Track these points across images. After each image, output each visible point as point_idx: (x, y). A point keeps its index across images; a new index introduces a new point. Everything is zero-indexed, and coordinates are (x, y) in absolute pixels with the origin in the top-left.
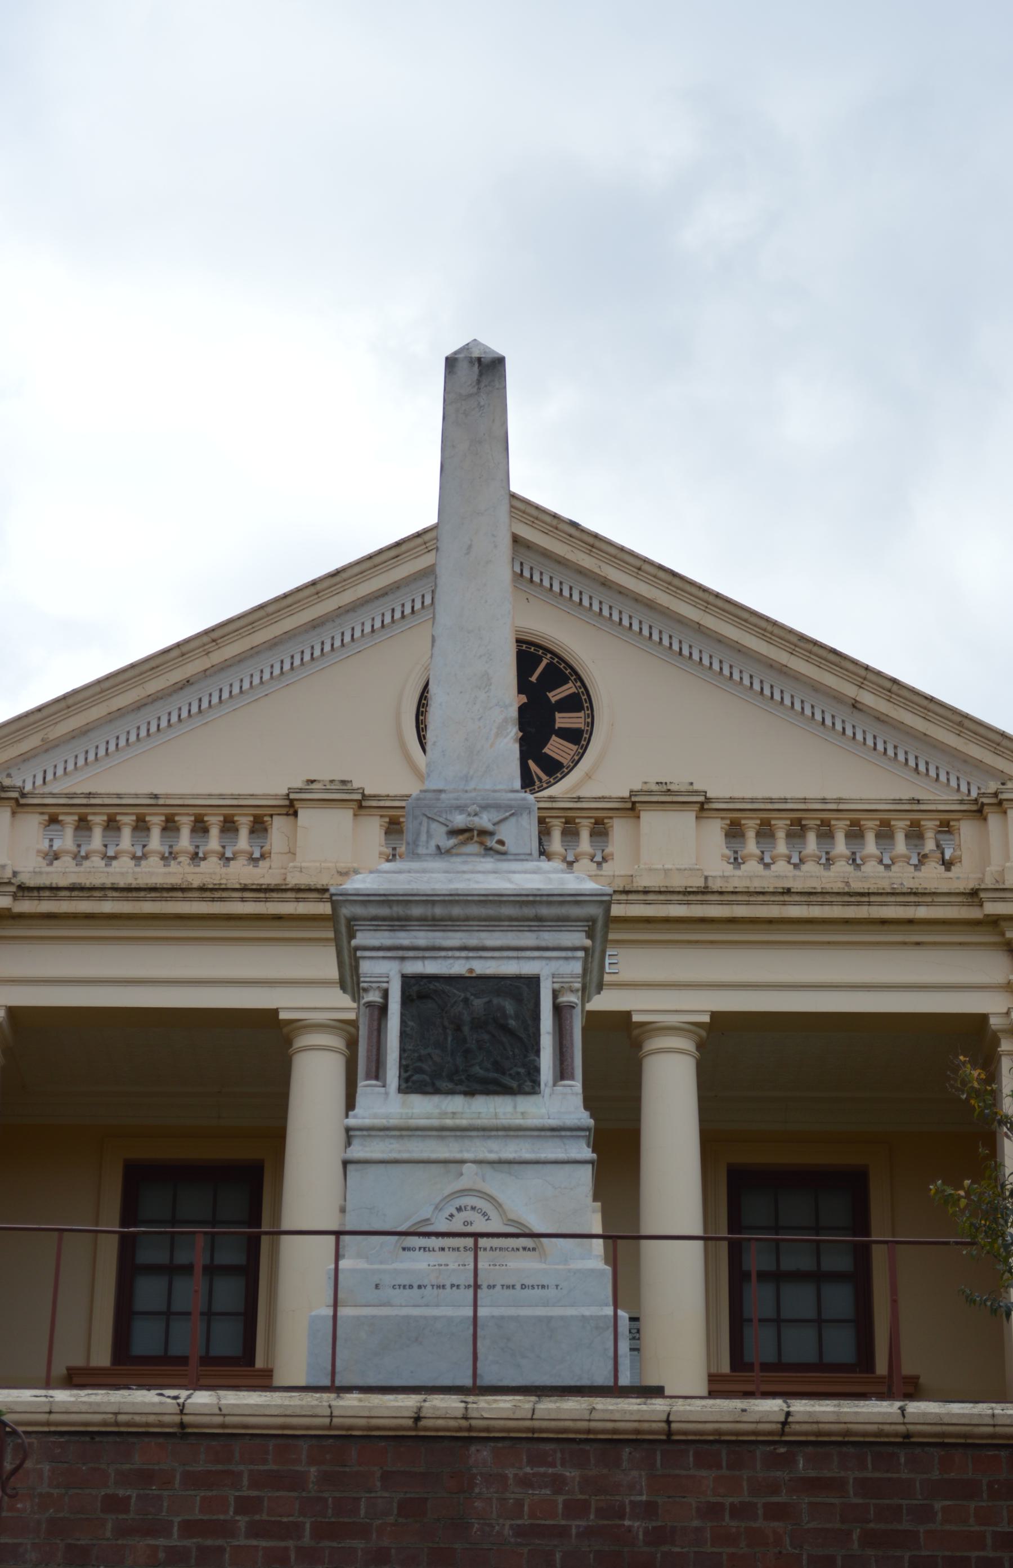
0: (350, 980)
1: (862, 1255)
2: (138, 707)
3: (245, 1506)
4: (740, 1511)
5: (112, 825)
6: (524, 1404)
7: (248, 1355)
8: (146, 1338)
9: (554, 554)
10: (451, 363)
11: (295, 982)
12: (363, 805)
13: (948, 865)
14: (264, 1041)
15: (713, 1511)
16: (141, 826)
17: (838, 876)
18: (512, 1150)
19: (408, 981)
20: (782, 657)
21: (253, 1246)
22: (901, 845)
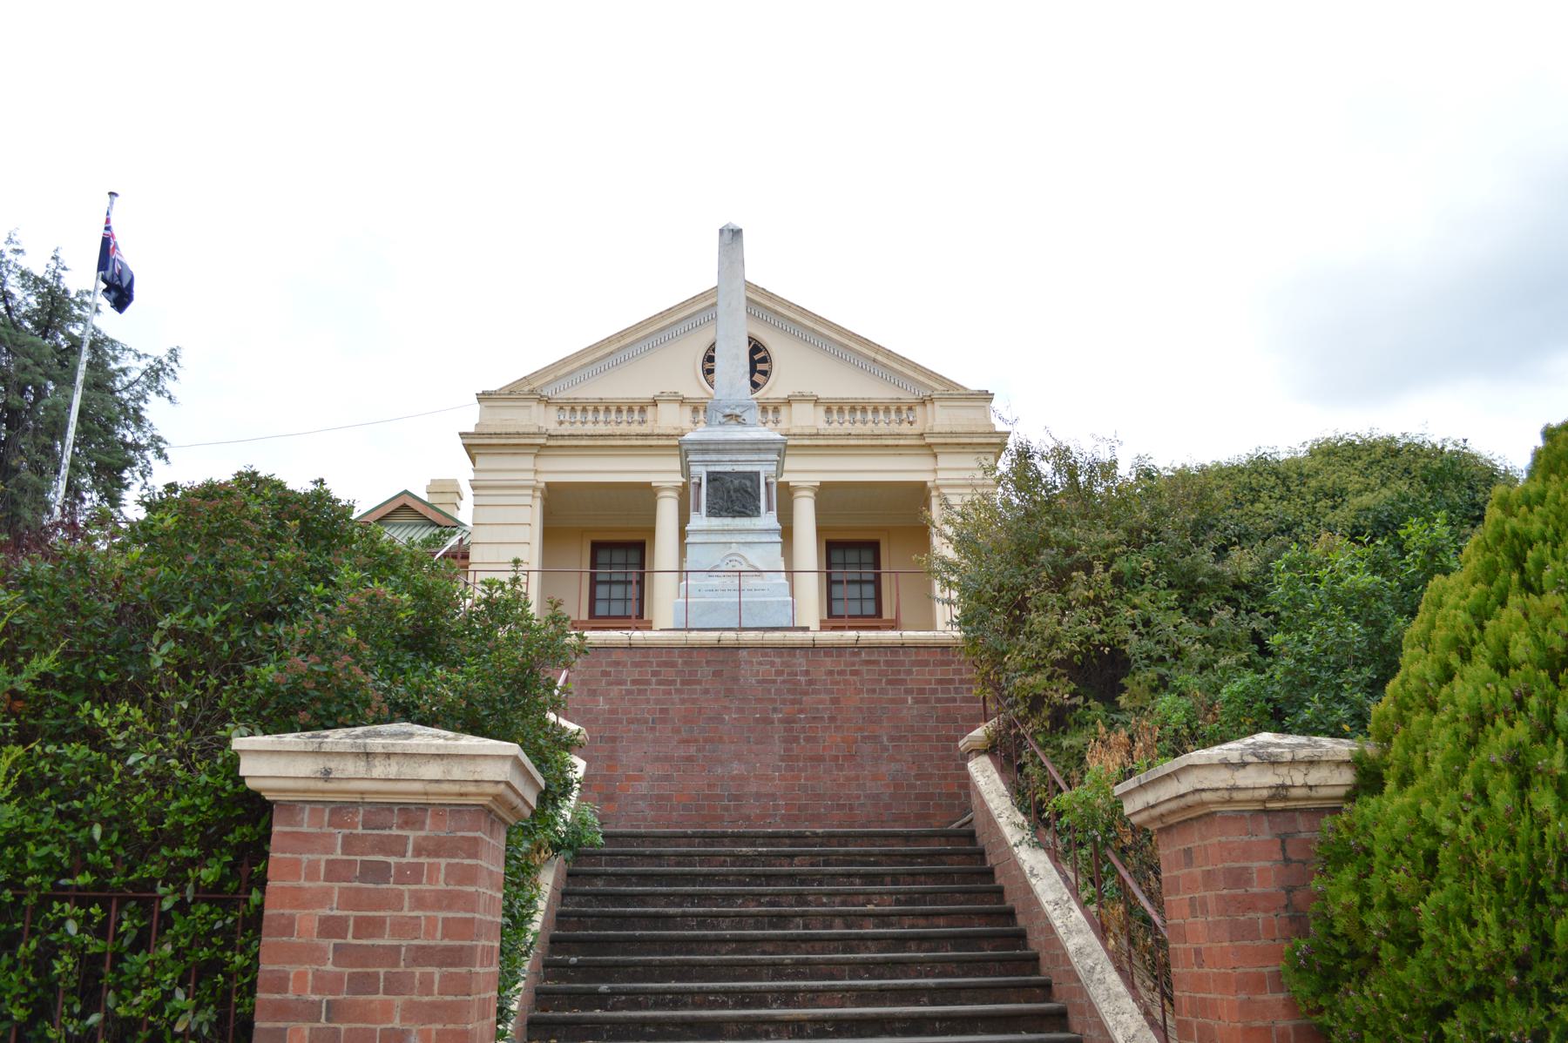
0: (686, 470)
1: (878, 577)
2: (593, 363)
3: (655, 674)
4: (841, 673)
5: (584, 410)
6: (759, 634)
7: (641, 615)
8: (601, 609)
9: (762, 305)
10: (721, 231)
11: (663, 473)
12: (683, 402)
13: (911, 423)
14: (645, 495)
15: (831, 673)
16: (596, 410)
17: (868, 428)
18: (750, 538)
19: (709, 474)
20: (846, 342)
21: (642, 575)
22: (893, 416)
